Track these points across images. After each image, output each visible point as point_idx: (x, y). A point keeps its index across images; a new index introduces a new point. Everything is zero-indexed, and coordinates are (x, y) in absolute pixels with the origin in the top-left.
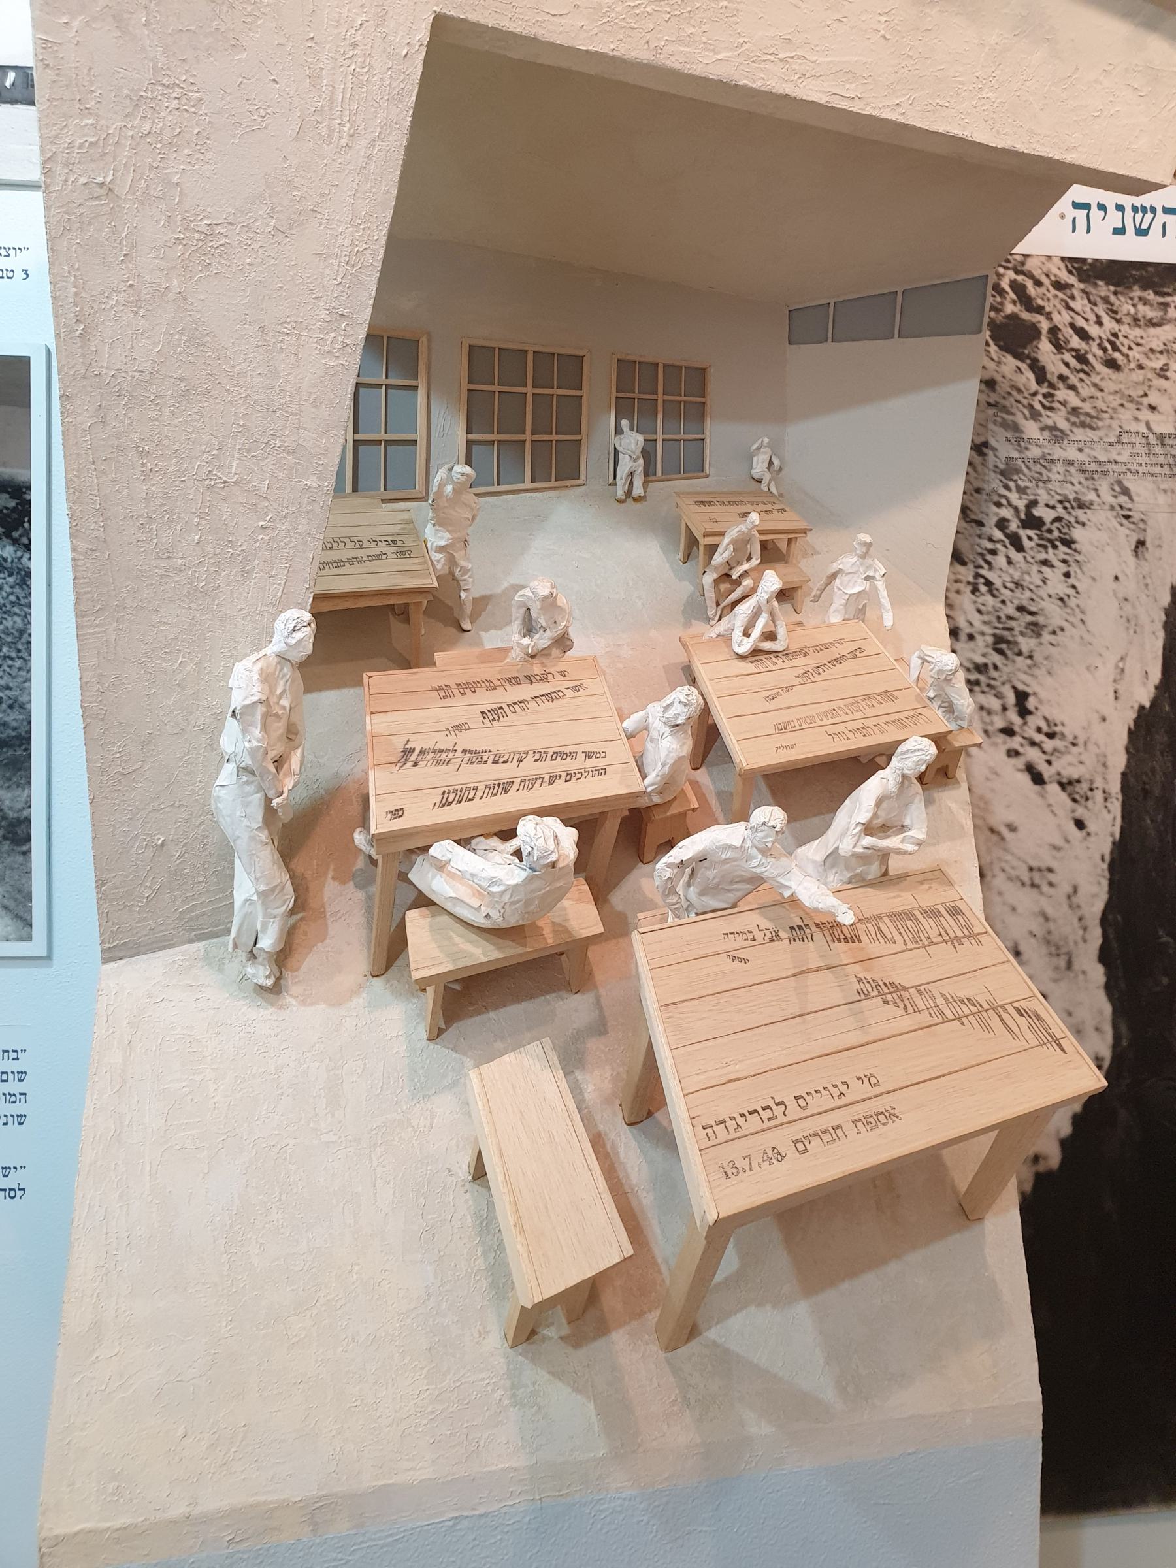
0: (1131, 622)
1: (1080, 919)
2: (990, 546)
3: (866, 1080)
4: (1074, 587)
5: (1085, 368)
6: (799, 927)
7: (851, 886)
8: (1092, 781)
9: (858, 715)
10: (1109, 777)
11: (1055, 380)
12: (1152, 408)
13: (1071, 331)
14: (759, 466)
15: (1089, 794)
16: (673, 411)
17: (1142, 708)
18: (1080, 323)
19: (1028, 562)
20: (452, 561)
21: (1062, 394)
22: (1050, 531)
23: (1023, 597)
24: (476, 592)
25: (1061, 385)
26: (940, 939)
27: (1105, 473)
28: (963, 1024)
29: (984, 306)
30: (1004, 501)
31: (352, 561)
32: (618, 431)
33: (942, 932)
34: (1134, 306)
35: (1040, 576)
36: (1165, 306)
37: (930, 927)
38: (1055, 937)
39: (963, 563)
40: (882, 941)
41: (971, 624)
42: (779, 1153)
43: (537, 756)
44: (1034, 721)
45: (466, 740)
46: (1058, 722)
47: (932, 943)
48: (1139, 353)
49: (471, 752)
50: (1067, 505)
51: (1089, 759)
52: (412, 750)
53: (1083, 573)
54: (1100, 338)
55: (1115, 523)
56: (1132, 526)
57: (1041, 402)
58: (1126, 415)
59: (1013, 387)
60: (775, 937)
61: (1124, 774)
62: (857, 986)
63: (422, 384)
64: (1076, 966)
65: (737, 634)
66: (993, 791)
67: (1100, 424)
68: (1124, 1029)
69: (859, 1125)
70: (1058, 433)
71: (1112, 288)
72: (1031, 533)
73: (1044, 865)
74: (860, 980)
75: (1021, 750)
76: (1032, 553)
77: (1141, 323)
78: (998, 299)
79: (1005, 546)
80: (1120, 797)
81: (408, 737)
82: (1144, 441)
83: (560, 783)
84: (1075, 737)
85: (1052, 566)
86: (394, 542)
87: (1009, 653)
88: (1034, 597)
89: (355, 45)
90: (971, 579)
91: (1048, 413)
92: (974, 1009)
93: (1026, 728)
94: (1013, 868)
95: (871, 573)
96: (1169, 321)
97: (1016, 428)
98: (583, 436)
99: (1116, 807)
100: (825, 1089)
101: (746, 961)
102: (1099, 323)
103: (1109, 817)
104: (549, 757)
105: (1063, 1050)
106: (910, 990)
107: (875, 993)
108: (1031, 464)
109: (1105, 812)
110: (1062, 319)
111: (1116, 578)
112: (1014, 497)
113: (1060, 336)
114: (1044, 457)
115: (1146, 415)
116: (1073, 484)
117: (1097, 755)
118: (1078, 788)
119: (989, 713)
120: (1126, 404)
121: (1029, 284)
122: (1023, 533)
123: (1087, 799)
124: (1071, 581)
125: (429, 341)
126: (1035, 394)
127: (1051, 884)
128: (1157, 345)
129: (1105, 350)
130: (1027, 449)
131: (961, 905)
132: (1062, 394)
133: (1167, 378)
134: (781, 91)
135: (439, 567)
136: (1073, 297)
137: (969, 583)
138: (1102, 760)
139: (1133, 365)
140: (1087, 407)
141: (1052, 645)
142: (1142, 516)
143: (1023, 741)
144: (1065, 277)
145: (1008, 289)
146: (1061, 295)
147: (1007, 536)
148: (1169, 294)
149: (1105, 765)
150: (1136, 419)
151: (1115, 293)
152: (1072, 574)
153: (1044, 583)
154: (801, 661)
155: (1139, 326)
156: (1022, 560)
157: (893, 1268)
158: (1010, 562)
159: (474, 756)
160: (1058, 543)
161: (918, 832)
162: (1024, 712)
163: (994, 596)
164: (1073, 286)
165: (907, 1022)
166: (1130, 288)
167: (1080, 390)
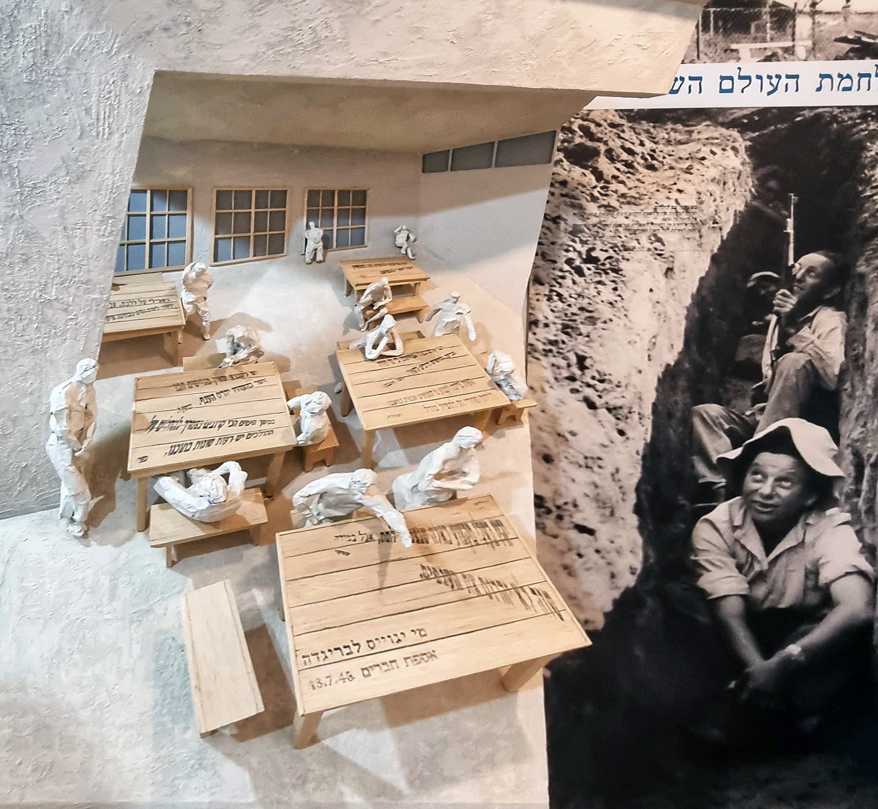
0: (663, 317)
1: (621, 488)
2: (561, 274)
3: (418, 632)
4: (619, 296)
5: (631, 170)
6: (387, 533)
7: (426, 506)
8: (631, 408)
9: (446, 395)
10: (643, 406)
11: (609, 178)
12: (680, 191)
13: (622, 151)
14: (401, 240)
15: (629, 415)
16: (343, 214)
17: (668, 365)
18: (628, 145)
19: (587, 282)
20: (197, 308)
21: (614, 186)
22: (603, 264)
23: (584, 303)
24: (214, 318)
25: (614, 181)
26: (484, 542)
27: (644, 231)
28: (491, 598)
29: (553, 147)
30: (571, 249)
31: (138, 312)
32: (308, 227)
33: (486, 537)
34: (667, 133)
35: (596, 290)
36: (690, 133)
37: (478, 534)
38: (603, 497)
39: (542, 284)
40: (443, 542)
41: (547, 318)
42: (351, 676)
43: (231, 424)
44: (589, 373)
45: (189, 415)
46: (606, 373)
47: (478, 545)
48: (671, 160)
49: (191, 422)
50: (616, 249)
51: (629, 395)
52: (157, 422)
53: (627, 288)
54: (642, 153)
55: (651, 258)
56: (664, 260)
57: (599, 192)
58: (661, 197)
59: (579, 184)
60: (370, 539)
61: (654, 404)
62: (421, 571)
63: (188, 212)
64: (618, 514)
65: (368, 348)
66: (560, 412)
67: (641, 202)
68: (651, 553)
69: (408, 660)
70: (610, 209)
71: (652, 124)
72: (590, 266)
73: (595, 456)
74: (423, 567)
75: (580, 389)
76: (590, 277)
77: (673, 143)
78: (570, 135)
79: (571, 274)
80: (651, 417)
81: (155, 414)
82: (674, 211)
83: (243, 439)
84: (619, 382)
85: (605, 284)
86: (164, 300)
87: (573, 334)
88: (591, 302)
89: (110, 92)
90: (547, 293)
91: (604, 198)
92: (501, 589)
93: (584, 377)
94: (573, 457)
95: (460, 311)
96: (694, 141)
97: (581, 207)
98: (286, 232)
99: (648, 423)
100: (389, 637)
101: (348, 554)
102: (642, 144)
103: (643, 429)
104: (238, 424)
105: (562, 619)
106: (458, 575)
107: (433, 576)
108: (591, 227)
109: (640, 426)
110: (615, 144)
111: (651, 290)
112: (578, 246)
113: (614, 154)
114: (600, 222)
115: (675, 195)
116: (620, 237)
117: (635, 393)
118: (620, 411)
119: (559, 367)
120: (661, 190)
121: (592, 126)
122: (584, 267)
123: (627, 418)
124: (618, 293)
125: (193, 191)
126: (595, 187)
127: (600, 467)
128: (684, 155)
129: (646, 160)
130: (588, 219)
131: (501, 519)
132: (614, 186)
133: (691, 174)
134: (382, 78)
135: (189, 311)
136: (623, 131)
137: (545, 295)
138: (638, 395)
139: (666, 167)
140: (633, 193)
141: (603, 329)
142: (671, 254)
143: (582, 384)
144: (618, 120)
145: (577, 129)
146: (615, 131)
147: (572, 268)
148: (693, 126)
149: (640, 398)
150: (668, 198)
151: (654, 127)
152: (619, 289)
153: (599, 294)
154: (411, 361)
155: (671, 145)
156: (583, 281)
157: (451, 716)
158: (574, 282)
159: (192, 424)
160: (609, 271)
161: (474, 477)
162: (582, 367)
163: (563, 302)
164: (623, 125)
165: (452, 596)
166: (665, 124)
167: (627, 183)
